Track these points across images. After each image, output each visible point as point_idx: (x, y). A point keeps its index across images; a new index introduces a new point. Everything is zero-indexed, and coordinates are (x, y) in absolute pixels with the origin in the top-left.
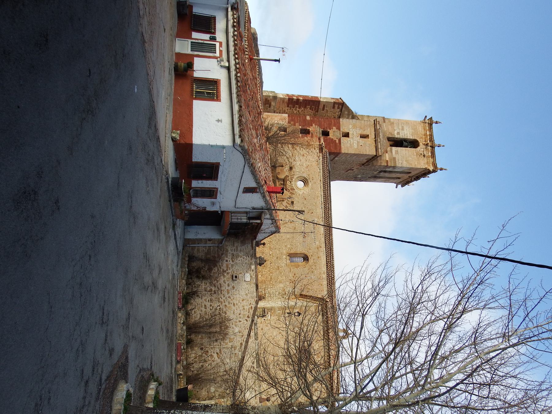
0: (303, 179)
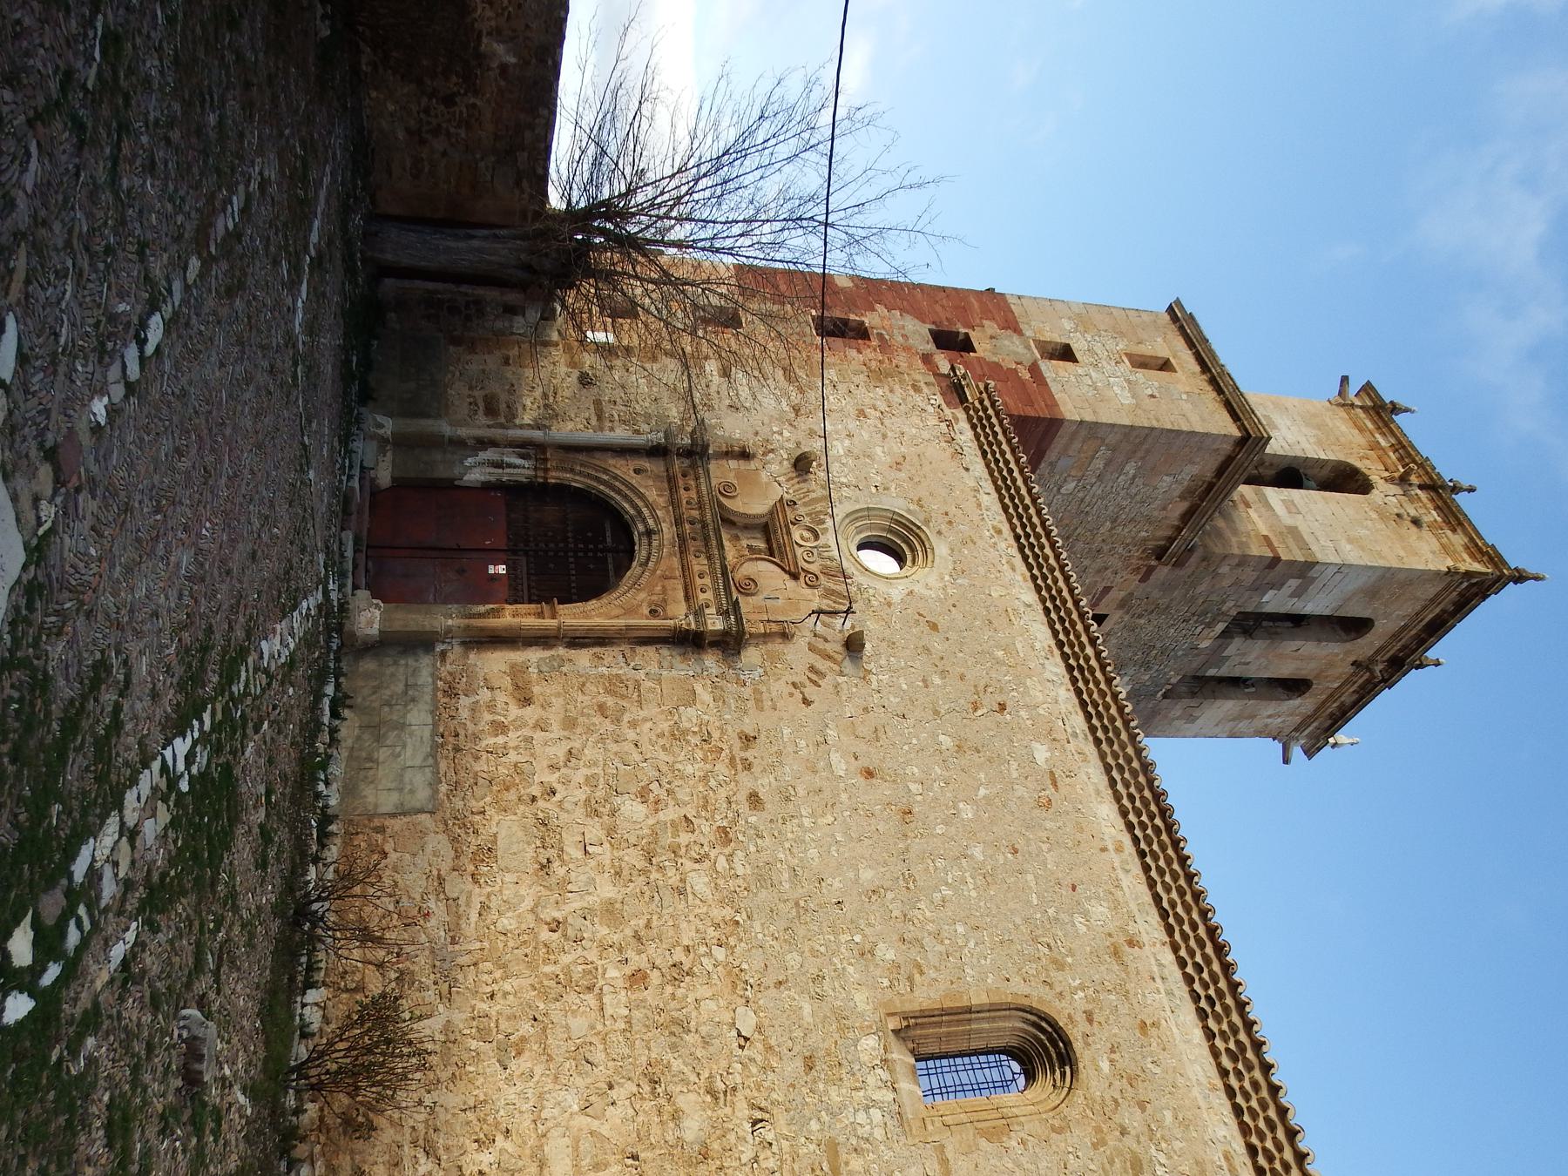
0: (890, 530)
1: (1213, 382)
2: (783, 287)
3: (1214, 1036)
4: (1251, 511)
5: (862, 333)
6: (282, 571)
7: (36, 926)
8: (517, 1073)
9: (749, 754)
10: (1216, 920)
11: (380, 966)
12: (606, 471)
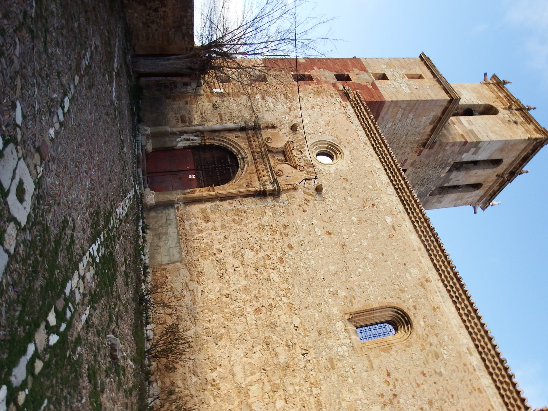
0: (327, 148)
1: (438, 81)
2: (281, 65)
3: (459, 309)
4: (455, 126)
5: (310, 78)
6: (120, 184)
7: (56, 311)
8: (221, 346)
9: (286, 231)
10: (456, 270)
11: (170, 315)
12: (225, 138)
